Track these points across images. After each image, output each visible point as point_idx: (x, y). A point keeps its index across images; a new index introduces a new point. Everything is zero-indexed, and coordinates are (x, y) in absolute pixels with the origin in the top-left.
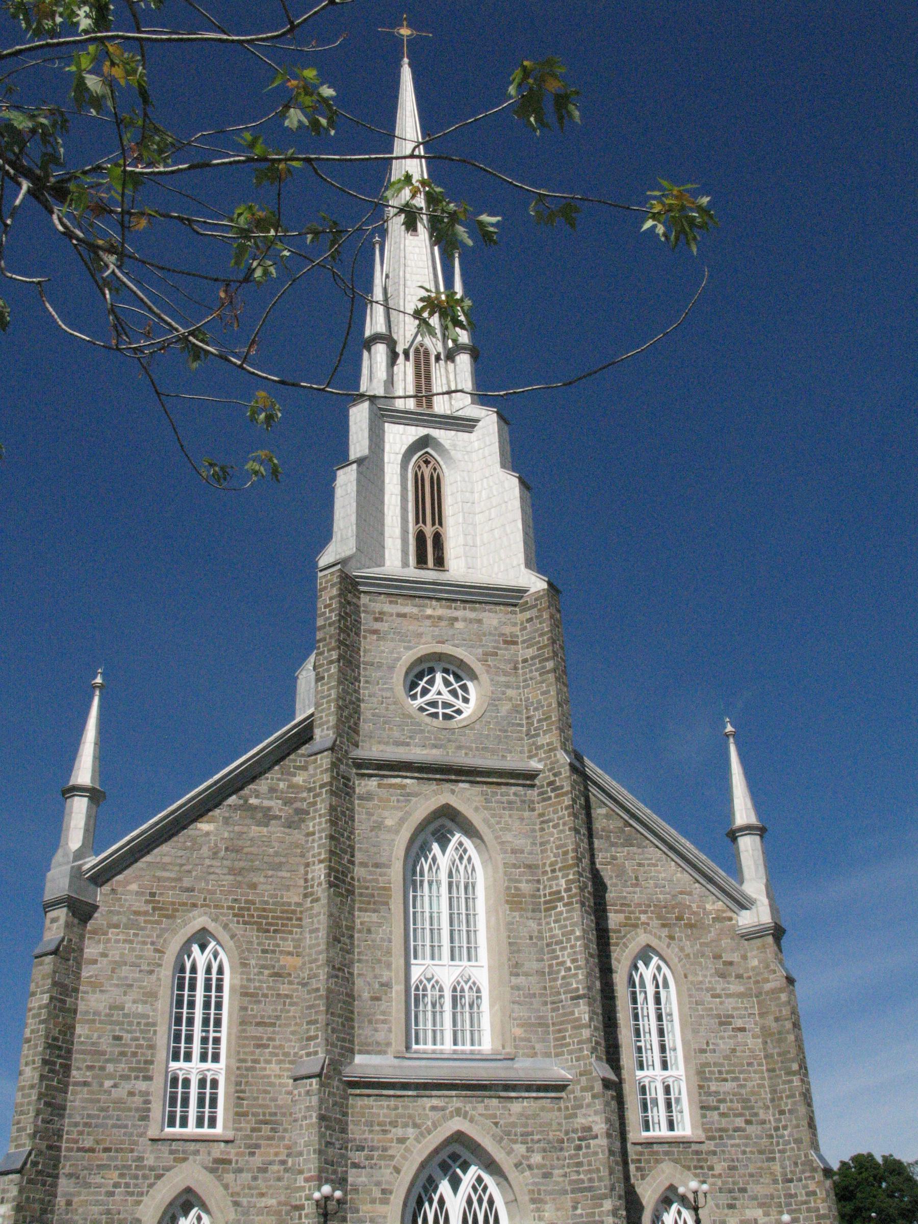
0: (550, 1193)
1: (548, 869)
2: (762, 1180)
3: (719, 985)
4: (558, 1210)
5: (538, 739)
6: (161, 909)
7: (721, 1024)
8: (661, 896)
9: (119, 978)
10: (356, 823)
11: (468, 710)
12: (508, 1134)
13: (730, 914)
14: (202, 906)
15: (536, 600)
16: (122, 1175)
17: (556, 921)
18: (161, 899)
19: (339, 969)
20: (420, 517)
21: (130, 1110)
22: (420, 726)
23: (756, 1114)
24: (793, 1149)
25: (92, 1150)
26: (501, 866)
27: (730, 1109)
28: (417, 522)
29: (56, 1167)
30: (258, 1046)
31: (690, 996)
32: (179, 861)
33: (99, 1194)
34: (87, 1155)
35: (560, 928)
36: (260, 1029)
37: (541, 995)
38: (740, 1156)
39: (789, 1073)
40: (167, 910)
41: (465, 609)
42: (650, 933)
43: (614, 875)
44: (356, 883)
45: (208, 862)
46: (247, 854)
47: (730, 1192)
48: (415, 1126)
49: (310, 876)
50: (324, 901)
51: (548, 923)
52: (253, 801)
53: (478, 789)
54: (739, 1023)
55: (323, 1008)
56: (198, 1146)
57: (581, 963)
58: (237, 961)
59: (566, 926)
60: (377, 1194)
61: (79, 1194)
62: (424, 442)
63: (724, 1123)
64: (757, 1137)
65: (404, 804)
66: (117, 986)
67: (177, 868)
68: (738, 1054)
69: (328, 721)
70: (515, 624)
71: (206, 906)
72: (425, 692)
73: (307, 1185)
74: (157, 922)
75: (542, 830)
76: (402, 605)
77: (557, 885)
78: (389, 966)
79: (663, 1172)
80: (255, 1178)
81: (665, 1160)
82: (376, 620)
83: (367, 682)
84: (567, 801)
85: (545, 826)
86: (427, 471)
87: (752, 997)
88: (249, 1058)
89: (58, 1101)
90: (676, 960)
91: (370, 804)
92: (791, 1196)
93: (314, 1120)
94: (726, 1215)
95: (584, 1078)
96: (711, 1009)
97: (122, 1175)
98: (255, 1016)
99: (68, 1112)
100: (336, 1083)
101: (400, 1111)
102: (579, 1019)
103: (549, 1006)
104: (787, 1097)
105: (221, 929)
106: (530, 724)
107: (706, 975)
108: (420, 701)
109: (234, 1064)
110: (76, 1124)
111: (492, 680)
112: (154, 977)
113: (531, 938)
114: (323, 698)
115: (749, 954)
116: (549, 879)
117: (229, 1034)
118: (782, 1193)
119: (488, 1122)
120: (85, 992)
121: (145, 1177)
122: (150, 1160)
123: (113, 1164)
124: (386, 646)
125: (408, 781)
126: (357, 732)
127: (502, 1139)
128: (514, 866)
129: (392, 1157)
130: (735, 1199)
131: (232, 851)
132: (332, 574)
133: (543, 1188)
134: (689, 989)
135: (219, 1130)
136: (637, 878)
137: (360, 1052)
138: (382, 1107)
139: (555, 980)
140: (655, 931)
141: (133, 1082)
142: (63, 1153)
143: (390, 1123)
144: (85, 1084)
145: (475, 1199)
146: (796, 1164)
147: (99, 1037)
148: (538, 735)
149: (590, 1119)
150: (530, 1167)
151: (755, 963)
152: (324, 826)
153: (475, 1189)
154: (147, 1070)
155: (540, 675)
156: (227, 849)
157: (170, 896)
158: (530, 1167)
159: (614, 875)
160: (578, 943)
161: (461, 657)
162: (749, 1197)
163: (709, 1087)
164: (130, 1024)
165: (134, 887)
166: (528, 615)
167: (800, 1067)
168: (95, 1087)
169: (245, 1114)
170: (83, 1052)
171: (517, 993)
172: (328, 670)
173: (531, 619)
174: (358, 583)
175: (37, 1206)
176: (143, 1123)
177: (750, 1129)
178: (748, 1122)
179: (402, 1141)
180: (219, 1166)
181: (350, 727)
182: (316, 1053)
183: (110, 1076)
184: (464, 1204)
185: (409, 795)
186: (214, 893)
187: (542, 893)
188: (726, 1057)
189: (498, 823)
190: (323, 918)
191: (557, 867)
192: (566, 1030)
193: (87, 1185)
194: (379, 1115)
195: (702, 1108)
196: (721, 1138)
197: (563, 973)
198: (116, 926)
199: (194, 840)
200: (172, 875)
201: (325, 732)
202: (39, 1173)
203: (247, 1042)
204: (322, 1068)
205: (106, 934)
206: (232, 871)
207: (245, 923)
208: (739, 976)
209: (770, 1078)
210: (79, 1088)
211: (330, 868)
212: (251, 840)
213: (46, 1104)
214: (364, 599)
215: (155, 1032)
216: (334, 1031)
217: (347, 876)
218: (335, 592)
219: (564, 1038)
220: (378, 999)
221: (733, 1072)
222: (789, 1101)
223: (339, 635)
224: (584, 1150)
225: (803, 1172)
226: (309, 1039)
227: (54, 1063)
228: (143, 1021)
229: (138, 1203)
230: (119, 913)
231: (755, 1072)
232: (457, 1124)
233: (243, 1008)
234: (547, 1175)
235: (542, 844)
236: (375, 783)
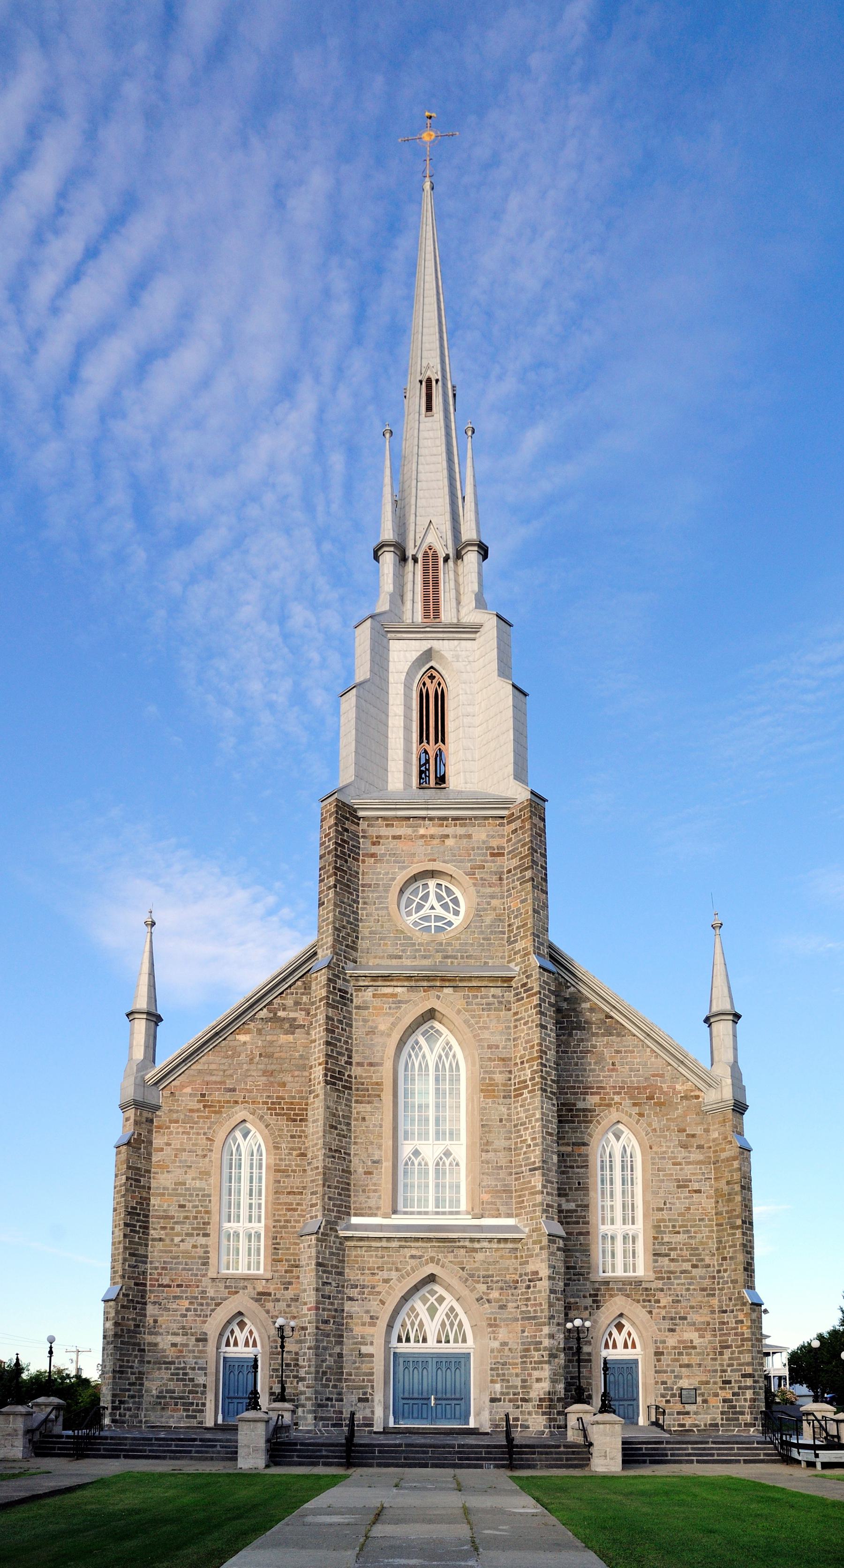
0: (505, 1320)
2: (701, 1311)
3: (681, 1154)
6: (210, 1106)
8: (635, 1079)
9: (180, 1161)
10: (354, 1030)
11: (457, 921)
12: (472, 1276)
13: (697, 1093)
15: (521, 811)
16: (191, 1303)
17: (521, 1106)
19: (336, 1151)
20: (423, 736)
21: (194, 1258)
23: (702, 1260)
24: (729, 1288)
25: (170, 1286)
26: (477, 1060)
27: (678, 1255)
28: (421, 742)
29: (143, 1297)
30: (289, 1210)
31: (653, 1164)
32: (222, 1067)
34: (166, 1289)
38: (684, 1293)
39: (734, 1227)
40: (215, 1106)
41: (455, 825)
44: (353, 1080)
46: (277, 1059)
47: (672, 1319)
48: (397, 1270)
49: (312, 1077)
50: (322, 1097)
51: (516, 1108)
52: (281, 1014)
54: (696, 1186)
55: (321, 1182)
57: (539, 1141)
58: (271, 1145)
59: (528, 1110)
61: (162, 1315)
62: (428, 655)
63: (673, 1266)
64: (701, 1278)
69: (327, 942)
70: (503, 836)
71: (246, 1102)
72: (420, 907)
75: (516, 1027)
78: (380, 1147)
79: (616, 1304)
80: (289, 1306)
82: (374, 844)
83: (365, 903)
84: (535, 1000)
85: (518, 1023)
86: (431, 687)
87: (710, 1164)
88: (283, 1219)
89: (141, 1252)
92: (724, 1323)
93: (314, 1267)
96: (672, 1175)
97: (191, 1303)
98: (286, 1188)
99: (149, 1260)
100: (332, 1239)
101: (386, 1258)
102: (535, 1187)
103: (513, 1176)
104: (730, 1247)
106: (511, 931)
107: (670, 1145)
108: (415, 917)
109: (271, 1223)
110: (156, 1268)
112: (207, 1159)
114: (323, 921)
116: (519, 1071)
117: (266, 1202)
118: (717, 1321)
120: (155, 1173)
121: (208, 1304)
122: (211, 1293)
123: (185, 1295)
124: (382, 868)
125: (399, 990)
126: (355, 949)
127: (467, 1280)
129: (379, 1293)
130: (676, 1325)
131: (265, 1057)
132: (330, 804)
133: (498, 1316)
135: (261, 1271)
136: (613, 1064)
137: (356, 1215)
138: (371, 1256)
139: (519, 1155)
141: (196, 1238)
142: (148, 1288)
143: (378, 1268)
144: (160, 1240)
145: (447, 1323)
146: (730, 1299)
147: (169, 1206)
148: (516, 941)
149: (538, 1266)
150: (489, 1301)
151: (716, 1135)
152: (322, 1034)
153: (447, 1315)
156: (261, 1055)
157: (217, 1096)
158: (489, 1301)
160: (537, 1124)
165: (188, 1090)
166: (513, 826)
167: (744, 1222)
168: (168, 1242)
169: (280, 1261)
170: (158, 1217)
172: (328, 895)
175: (132, 1323)
177: (695, 1272)
178: (695, 1266)
179: (386, 1281)
181: (347, 946)
182: (316, 1216)
183: (178, 1235)
184: (439, 1326)
186: (251, 1091)
187: (513, 1082)
190: (321, 1111)
192: (524, 1195)
196: (669, 1278)
197: (525, 1149)
198: (177, 1122)
199: (234, 1049)
200: (218, 1079)
201: (326, 952)
202: (130, 1301)
204: (320, 1228)
206: (265, 1073)
207: (276, 1114)
208: (700, 1147)
212: (280, 1047)
213: (130, 1254)
214: (363, 825)
215: (210, 1201)
216: (330, 1199)
218: (332, 821)
220: (370, 1173)
221: (686, 1226)
222: (731, 1250)
223: (336, 862)
224: (532, 1289)
225: (735, 1305)
226: (312, 1206)
227: (135, 1226)
228: (200, 1193)
229: (205, 1322)
230: (177, 1111)
234: (502, 1307)
235: (514, 1040)
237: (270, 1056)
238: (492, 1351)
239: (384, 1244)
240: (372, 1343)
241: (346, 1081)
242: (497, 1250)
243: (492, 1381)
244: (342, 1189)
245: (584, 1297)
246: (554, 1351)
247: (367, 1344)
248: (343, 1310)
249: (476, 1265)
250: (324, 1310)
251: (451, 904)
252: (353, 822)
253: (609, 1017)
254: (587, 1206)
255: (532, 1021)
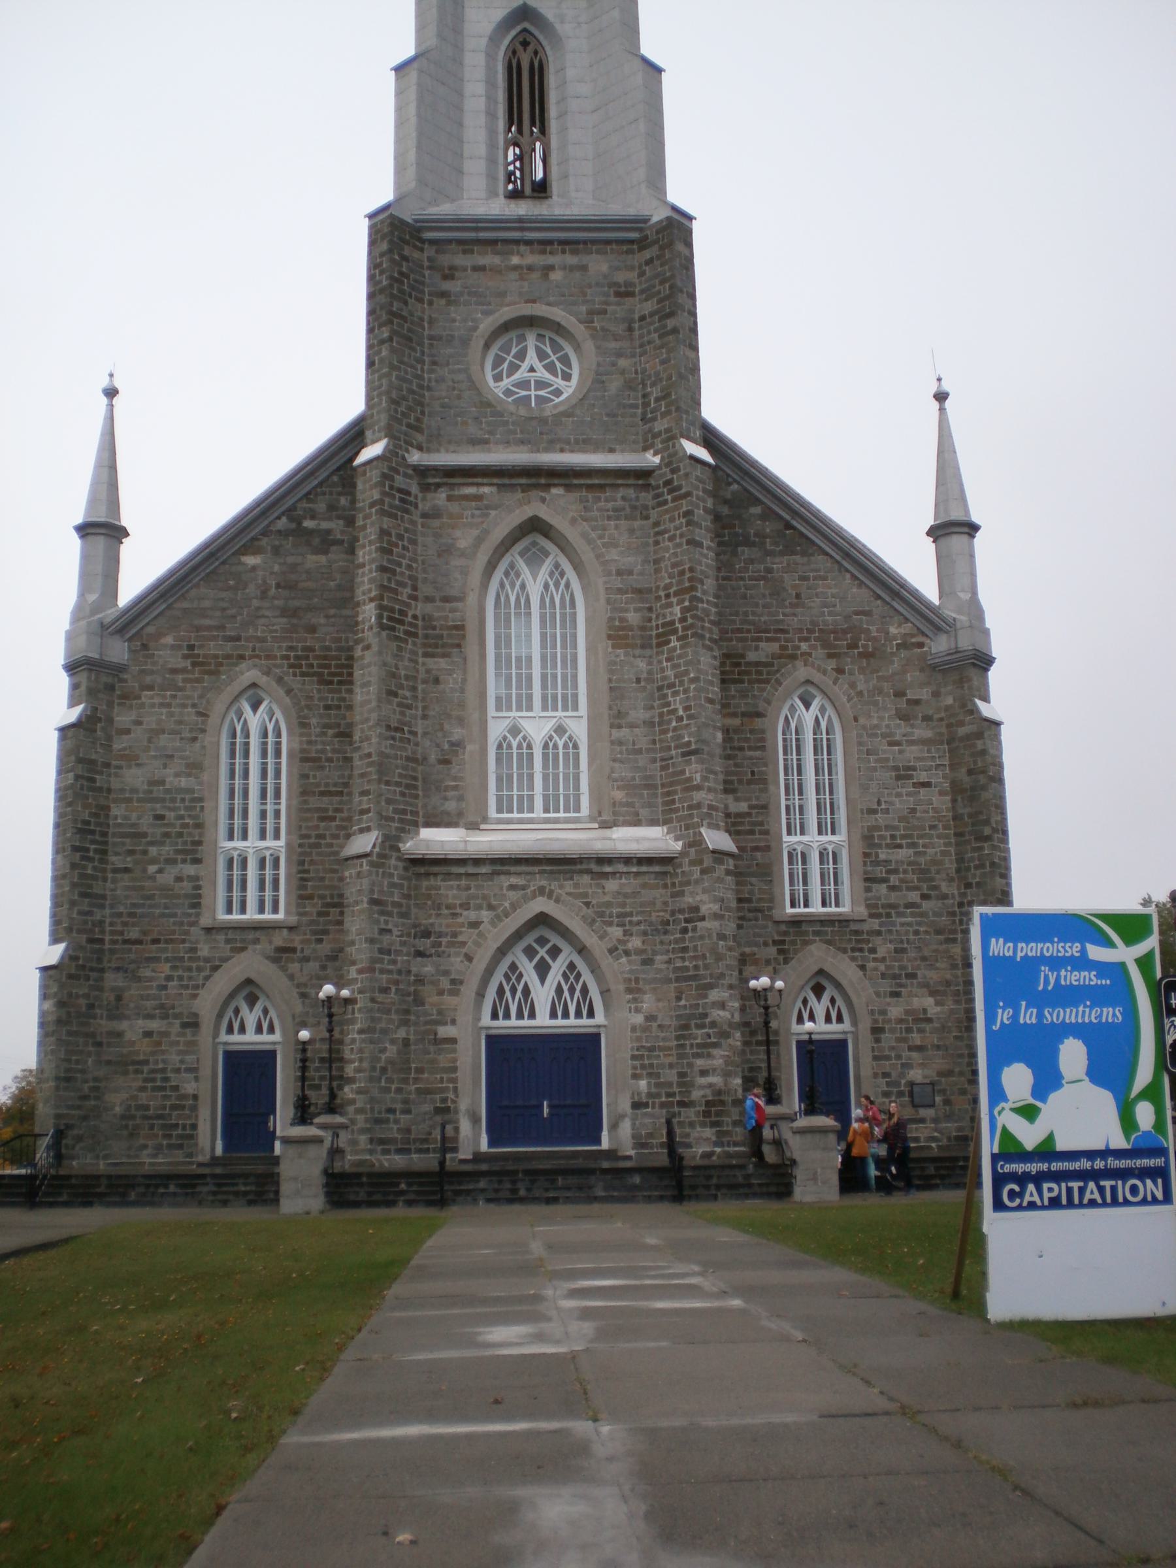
1: (662, 593)
3: (900, 730)
4: (659, 1000)
5: (656, 424)
7: (898, 778)
13: (921, 639)
14: (251, 657)
16: (174, 968)
17: (668, 660)
18: (201, 652)
19: (397, 729)
21: (178, 897)
22: (502, 416)
25: (140, 942)
27: (902, 881)
30: (322, 819)
31: (860, 744)
33: (151, 987)
34: (134, 947)
35: (674, 667)
36: (325, 799)
37: (648, 750)
38: (911, 937)
40: (210, 664)
41: (564, 252)
42: (813, 666)
43: (767, 593)
45: (255, 603)
48: (491, 907)
51: (660, 662)
53: (575, 495)
54: (923, 777)
56: (258, 934)
59: (679, 666)
60: (445, 983)
63: (894, 898)
64: (935, 914)
65: (480, 520)
66: (155, 757)
67: (218, 613)
68: (918, 815)
72: (514, 368)
73: (359, 977)
74: (198, 681)
75: (657, 543)
76: (479, 253)
77: (671, 613)
80: (324, 968)
81: (815, 941)
82: (446, 277)
85: (660, 538)
88: (313, 833)
90: (845, 699)
91: (436, 523)
94: (889, 1004)
95: (693, 850)
96: (887, 760)
97: (174, 968)
98: (318, 785)
100: (393, 862)
101: (472, 891)
102: (690, 779)
104: (976, 867)
105: (274, 684)
106: (646, 405)
111: (598, 348)
112: (198, 745)
113: (638, 680)
115: (943, 690)
116: (662, 607)
118: (961, 980)
119: (578, 902)
121: (199, 969)
125: (486, 490)
127: (594, 921)
128: (620, 591)
129: (464, 944)
130: (901, 986)
131: (284, 588)
134: (859, 736)
135: (281, 916)
136: (798, 596)
138: (451, 887)
139: (665, 732)
140: (817, 662)
143: (461, 905)
145: (565, 988)
147: (139, 818)
148: (654, 419)
150: (627, 953)
151: (949, 701)
152: (374, 555)
153: (565, 976)
154: (195, 852)
155: (660, 337)
156: (278, 586)
157: (212, 648)
159: (767, 593)
161: (558, 319)
162: (919, 983)
163: (877, 855)
164: (173, 800)
165: (169, 640)
166: (647, 254)
169: (311, 897)
171: (618, 749)
173: (649, 262)
174: (420, 230)
175: (82, 1002)
176: (193, 911)
177: (926, 905)
178: (924, 897)
179: (475, 925)
180: (282, 955)
181: (409, 426)
183: (154, 861)
184: (553, 993)
185: (488, 507)
188: (901, 819)
189: (601, 537)
191: (672, 591)
192: (675, 792)
193: (139, 979)
194: (447, 896)
195: (867, 880)
197: (674, 724)
198: (150, 688)
203: (308, 815)
205: (139, 697)
206: (284, 612)
207: (303, 674)
208: (927, 718)
209: (957, 844)
210: (118, 876)
211: (381, 607)
215: (202, 807)
217: (406, 616)
219: (673, 802)
222: (978, 872)
224: (690, 934)
228: (187, 797)
229: (195, 996)
230: (152, 672)
231: (939, 837)
232: (540, 905)
233: (305, 776)
234: (648, 962)
235: (656, 562)
236: (444, 495)
237: (291, 586)
238: (634, 1029)
239: (471, 869)
240: (453, 1022)
241: (410, 624)
242: (637, 874)
243: (635, 1076)
244: (408, 786)
245: (766, 944)
246: (725, 1027)
247: (445, 1024)
248: (409, 972)
249: (607, 898)
250: (382, 971)
251: (558, 365)
252: (415, 247)
253: (788, 526)
254: (765, 807)
255: (681, 536)
